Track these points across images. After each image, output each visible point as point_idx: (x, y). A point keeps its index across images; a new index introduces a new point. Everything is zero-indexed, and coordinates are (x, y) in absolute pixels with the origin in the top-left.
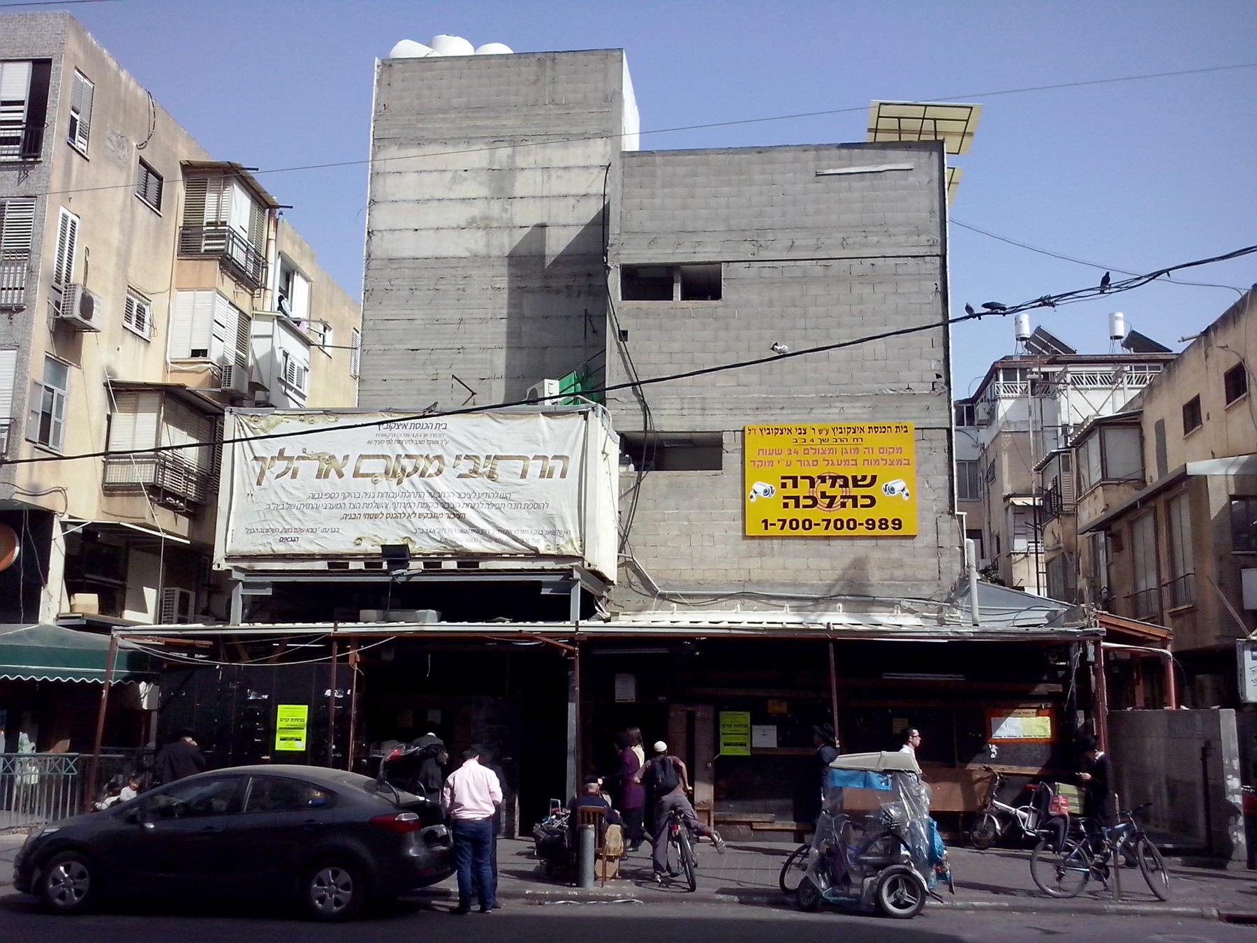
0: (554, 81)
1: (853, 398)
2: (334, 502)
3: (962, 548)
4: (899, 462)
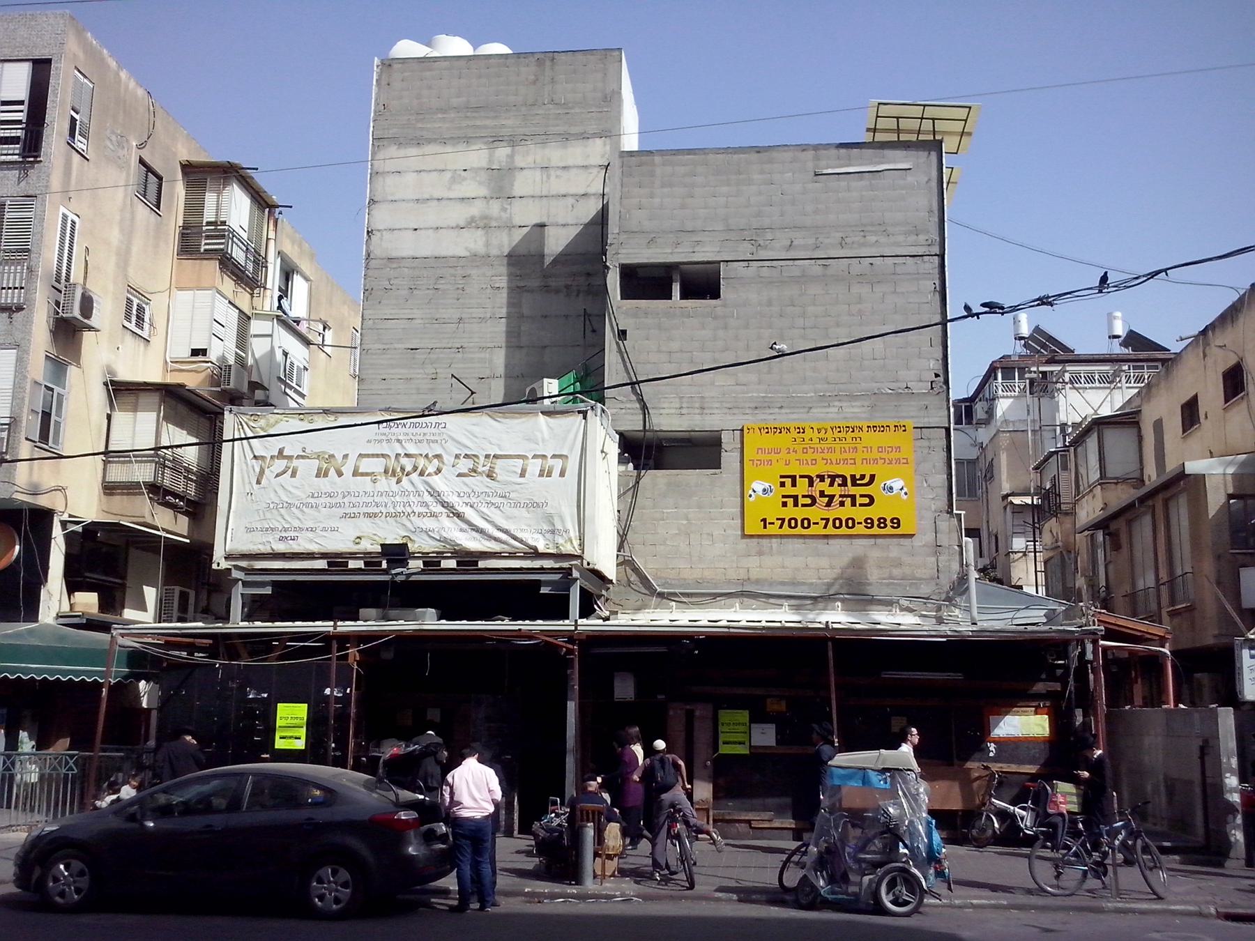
0: (553, 81)
1: (852, 397)
2: (333, 501)
3: (960, 546)
4: (898, 461)
